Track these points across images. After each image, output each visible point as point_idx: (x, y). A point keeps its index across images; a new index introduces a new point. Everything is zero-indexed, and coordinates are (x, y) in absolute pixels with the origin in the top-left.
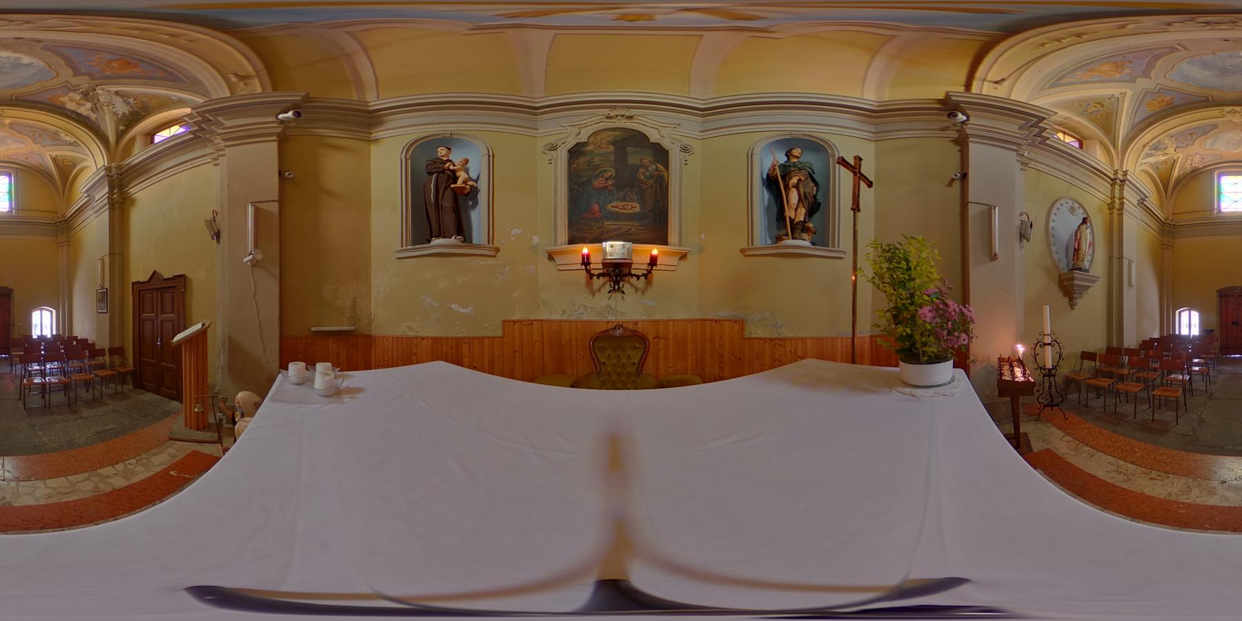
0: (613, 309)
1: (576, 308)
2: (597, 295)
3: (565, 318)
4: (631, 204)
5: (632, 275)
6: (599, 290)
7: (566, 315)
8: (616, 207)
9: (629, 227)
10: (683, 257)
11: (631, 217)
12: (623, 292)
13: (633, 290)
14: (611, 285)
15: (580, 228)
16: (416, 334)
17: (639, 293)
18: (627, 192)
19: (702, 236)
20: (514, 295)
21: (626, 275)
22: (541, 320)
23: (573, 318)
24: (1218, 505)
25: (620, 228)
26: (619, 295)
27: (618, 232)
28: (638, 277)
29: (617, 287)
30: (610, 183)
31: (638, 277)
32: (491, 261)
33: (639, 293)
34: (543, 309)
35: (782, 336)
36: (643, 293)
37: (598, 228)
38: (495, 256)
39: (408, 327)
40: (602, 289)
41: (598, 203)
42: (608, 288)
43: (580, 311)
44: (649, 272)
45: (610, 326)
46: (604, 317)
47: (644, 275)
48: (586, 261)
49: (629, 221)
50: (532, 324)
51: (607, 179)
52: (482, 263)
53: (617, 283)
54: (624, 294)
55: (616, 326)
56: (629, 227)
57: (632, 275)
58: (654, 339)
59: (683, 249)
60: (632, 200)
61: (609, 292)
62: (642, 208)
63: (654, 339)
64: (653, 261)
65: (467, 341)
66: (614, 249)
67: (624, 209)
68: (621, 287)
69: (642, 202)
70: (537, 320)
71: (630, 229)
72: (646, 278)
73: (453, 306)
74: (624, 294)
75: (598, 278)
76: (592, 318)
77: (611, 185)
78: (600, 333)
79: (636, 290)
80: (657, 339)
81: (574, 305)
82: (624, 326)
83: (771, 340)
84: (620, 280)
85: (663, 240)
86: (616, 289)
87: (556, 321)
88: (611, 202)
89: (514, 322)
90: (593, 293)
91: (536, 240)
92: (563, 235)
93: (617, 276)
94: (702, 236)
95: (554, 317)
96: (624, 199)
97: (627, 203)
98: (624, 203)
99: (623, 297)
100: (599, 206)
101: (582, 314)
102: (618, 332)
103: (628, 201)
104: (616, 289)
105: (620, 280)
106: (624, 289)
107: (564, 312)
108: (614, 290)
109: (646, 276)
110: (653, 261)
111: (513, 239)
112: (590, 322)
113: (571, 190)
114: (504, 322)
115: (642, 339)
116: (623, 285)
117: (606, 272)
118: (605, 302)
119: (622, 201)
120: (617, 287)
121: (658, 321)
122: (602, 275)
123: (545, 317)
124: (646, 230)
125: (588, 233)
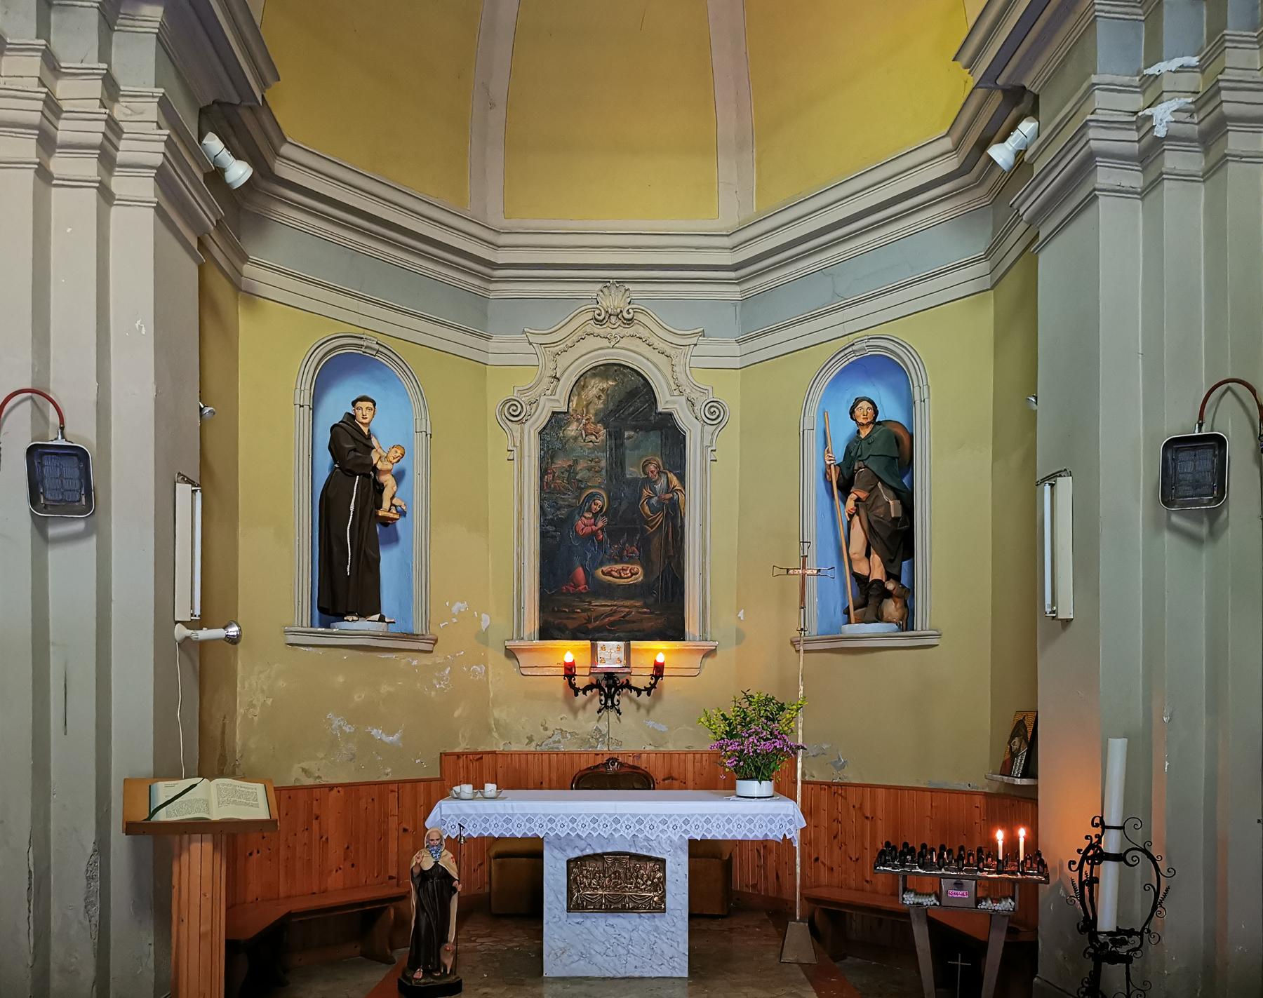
0: (604, 735)
1: (549, 733)
2: (581, 715)
3: (532, 748)
4: (630, 567)
5: (631, 688)
6: (584, 707)
7: (534, 744)
8: (609, 574)
9: (627, 610)
10: (710, 653)
11: (630, 592)
12: (619, 712)
13: (634, 707)
14: (601, 701)
15: (556, 609)
16: (318, 782)
17: (643, 711)
18: (624, 544)
19: (741, 614)
20: (456, 714)
21: (622, 687)
22: (494, 753)
23: (544, 748)
24: (918, 950)
25: (615, 612)
26: (613, 714)
27: (612, 619)
28: (639, 692)
29: (609, 703)
30: (600, 524)
31: (639, 692)
32: (426, 660)
33: (643, 711)
34: (495, 735)
35: (846, 781)
36: (648, 711)
37: (584, 611)
38: (432, 652)
39: (304, 770)
40: (589, 706)
41: (583, 566)
42: (596, 704)
43: (556, 738)
44: (653, 686)
45: (600, 760)
46: (592, 747)
47: (646, 689)
48: (570, 671)
49: (627, 599)
50: (481, 758)
51: (595, 515)
52: (415, 663)
53: (609, 696)
54: (620, 714)
55: (608, 760)
56: (627, 610)
57: (631, 688)
58: (664, 780)
59: (709, 645)
60: (631, 560)
61: (599, 711)
62: (645, 575)
63: (664, 780)
64: (659, 669)
65: (395, 787)
66: (610, 654)
67: (621, 577)
68: (616, 703)
69: (646, 563)
70: (488, 753)
71: (629, 613)
72: (649, 694)
73: (374, 732)
74: (620, 714)
75: (585, 693)
76: (574, 749)
77: (601, 529)
78: (586, 769)
79: (639, 706)
80: (670, 781)
81: (546, 729)
82: (620, 759)
83: (829, 785)
84: (615, 692)
85: (675, 631)
86: (609, 704)
87: (520, 754)
88: (602, 564)
89: (458, 755)
90: (574, 711)
91: (486, 621)
92: (531, 621)
93: (609, 687)
94: (741, 614)
95: (515, 747)
96: (620, 560)
97: (625, 566)
98: (619, 567)
99: (618, 719)
100: (585, 570)
101: (559, 742)
102: (612, 768)
103: (626, 563)
104: (609, 704)
105: (615, 692)
106: (621, 707)
107: (531, 739)
108: (606, 707)
109: (648, 690)
110: (659, 669)
111: (455, 620)
112: (571, 754)
113: (544, 535)
114: (444, 755)
115: (645, 777)
116: (618, 701)
117: (595, 683)
118: (593, 725)
119: (616, 563)
120: (609, 703)
121: (671, 754)
122: (590, 687)
123: (500, 748)
124: (651, 613)
125: (568, 618)
